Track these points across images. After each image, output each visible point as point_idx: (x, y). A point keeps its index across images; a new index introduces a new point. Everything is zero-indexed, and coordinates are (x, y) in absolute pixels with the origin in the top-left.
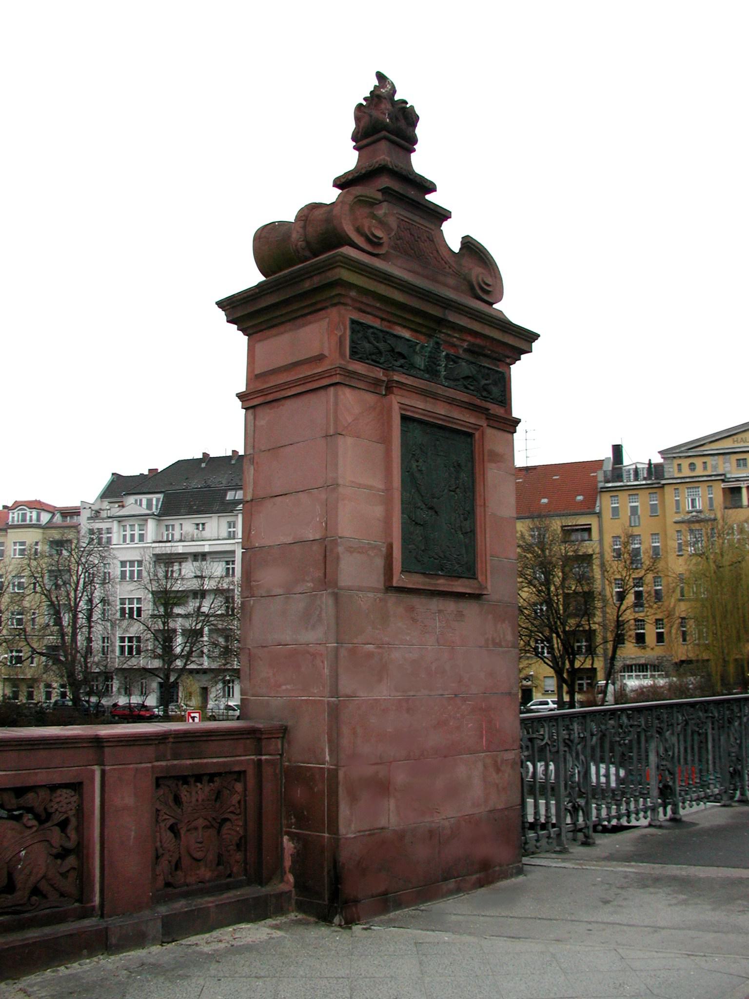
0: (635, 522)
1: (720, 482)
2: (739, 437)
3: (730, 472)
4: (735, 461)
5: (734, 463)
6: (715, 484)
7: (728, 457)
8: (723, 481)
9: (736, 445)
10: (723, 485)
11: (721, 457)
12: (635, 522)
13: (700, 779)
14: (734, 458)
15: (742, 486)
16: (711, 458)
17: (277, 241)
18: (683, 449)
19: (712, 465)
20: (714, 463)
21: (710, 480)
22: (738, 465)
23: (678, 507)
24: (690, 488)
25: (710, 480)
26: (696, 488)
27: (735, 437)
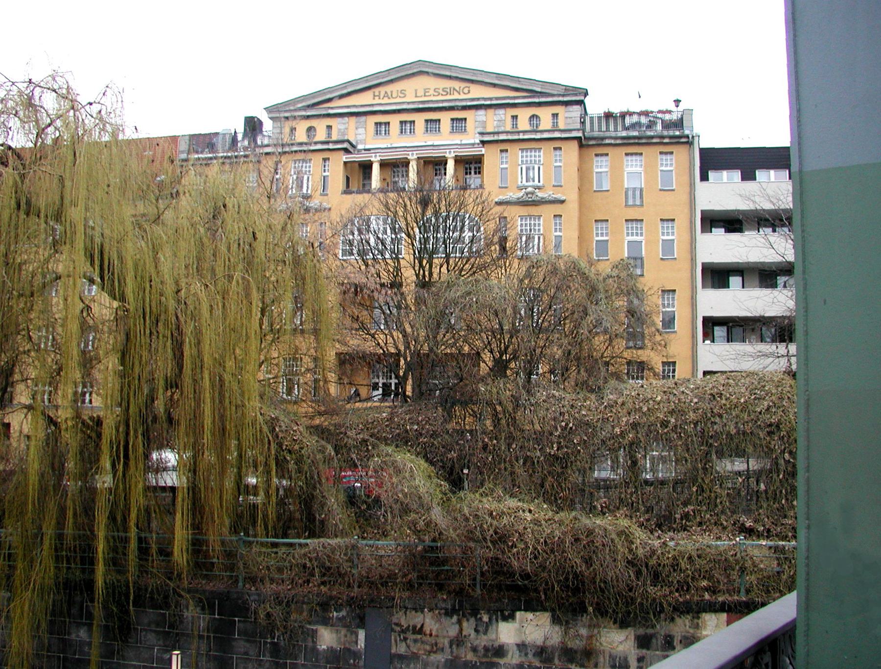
0: (634, 197)
1: (342, 152)
2: (382, 90)
3: (364, 142)
4: (449, 121)
5: (371, 127)
6: (332, 156)
7: (363, 119)
8: (346, 150)
9: (377, 101)
10: (345, 158)
11: (353, 120)
12: (634, 197)
13: (459, 400)
14: (372, 120)
15: (372, 159)
16: (339, 120)
17: (108, 518)
18: (300, 105)
19: (339, 130)
20: (342, 127)
21: (328, 149)
22: (377, 133)
23: (503, 178)
24: (527, 150)
25: (328, 149)
26: (535, 149)
27: (377, 90)
